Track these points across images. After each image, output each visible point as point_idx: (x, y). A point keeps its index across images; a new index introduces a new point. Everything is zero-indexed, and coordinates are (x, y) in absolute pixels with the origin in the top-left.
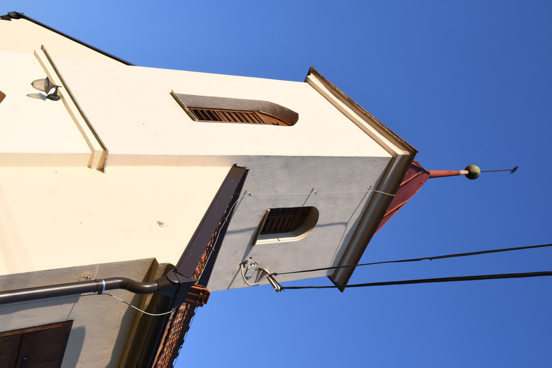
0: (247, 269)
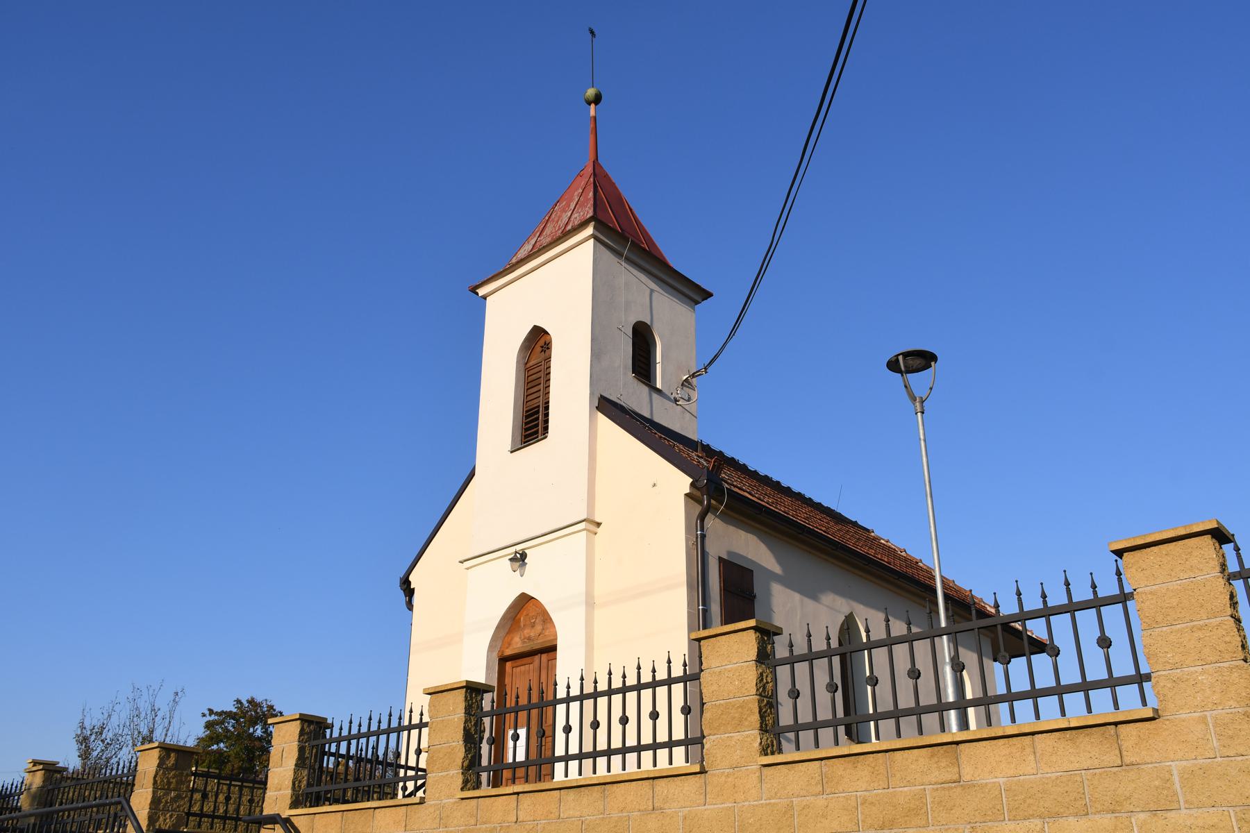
0: (681, 398)
